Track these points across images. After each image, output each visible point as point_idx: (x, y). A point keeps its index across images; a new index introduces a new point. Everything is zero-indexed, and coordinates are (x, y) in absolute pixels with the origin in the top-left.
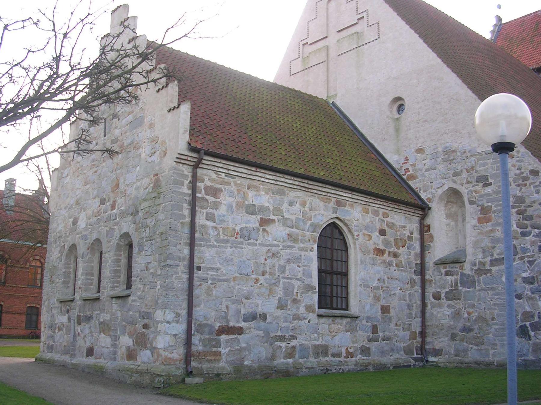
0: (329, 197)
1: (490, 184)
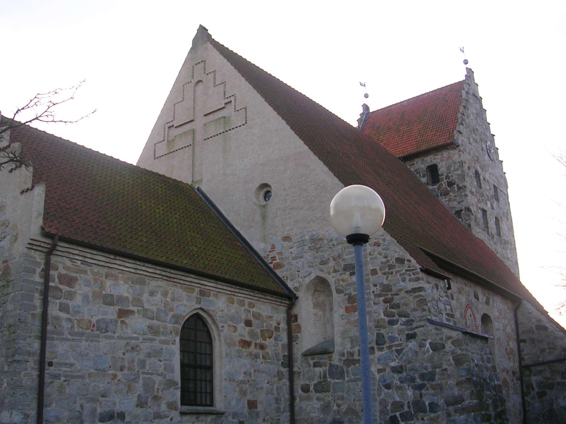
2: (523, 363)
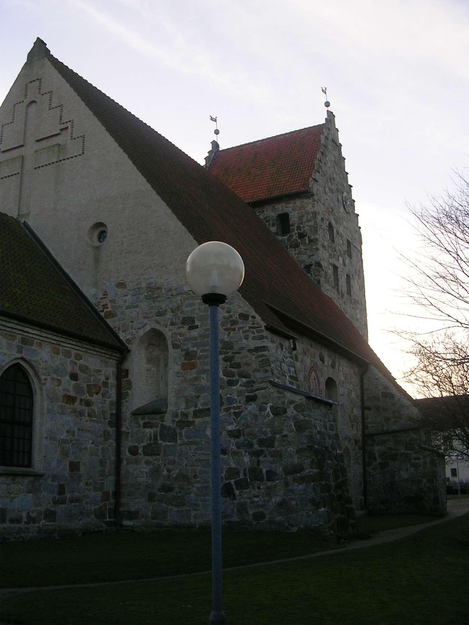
0: (13, 334)
1: (197, 327)
2: (366, 432)
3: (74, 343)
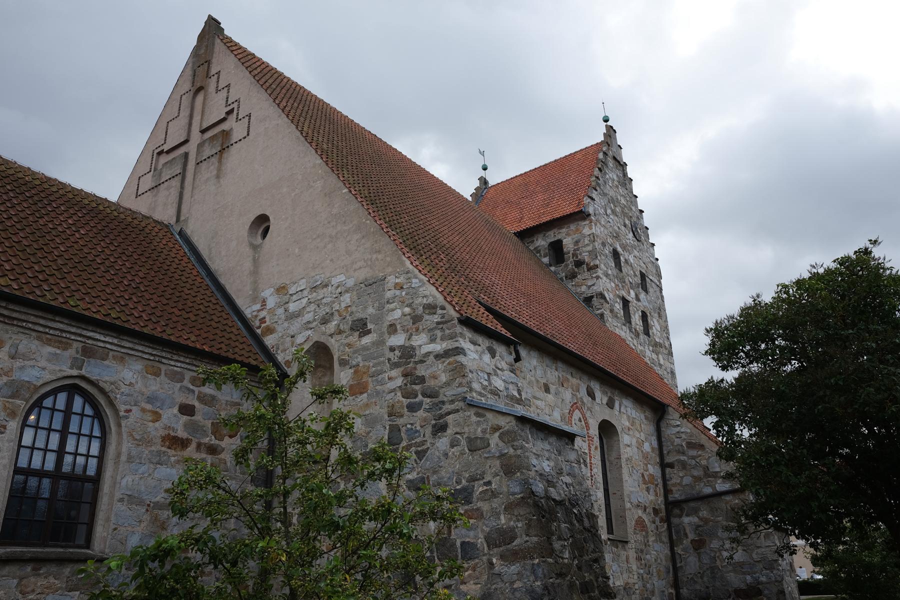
0: (64, 340)
1: (369, 332)
2: (671, 498)
3: (188, 361)
